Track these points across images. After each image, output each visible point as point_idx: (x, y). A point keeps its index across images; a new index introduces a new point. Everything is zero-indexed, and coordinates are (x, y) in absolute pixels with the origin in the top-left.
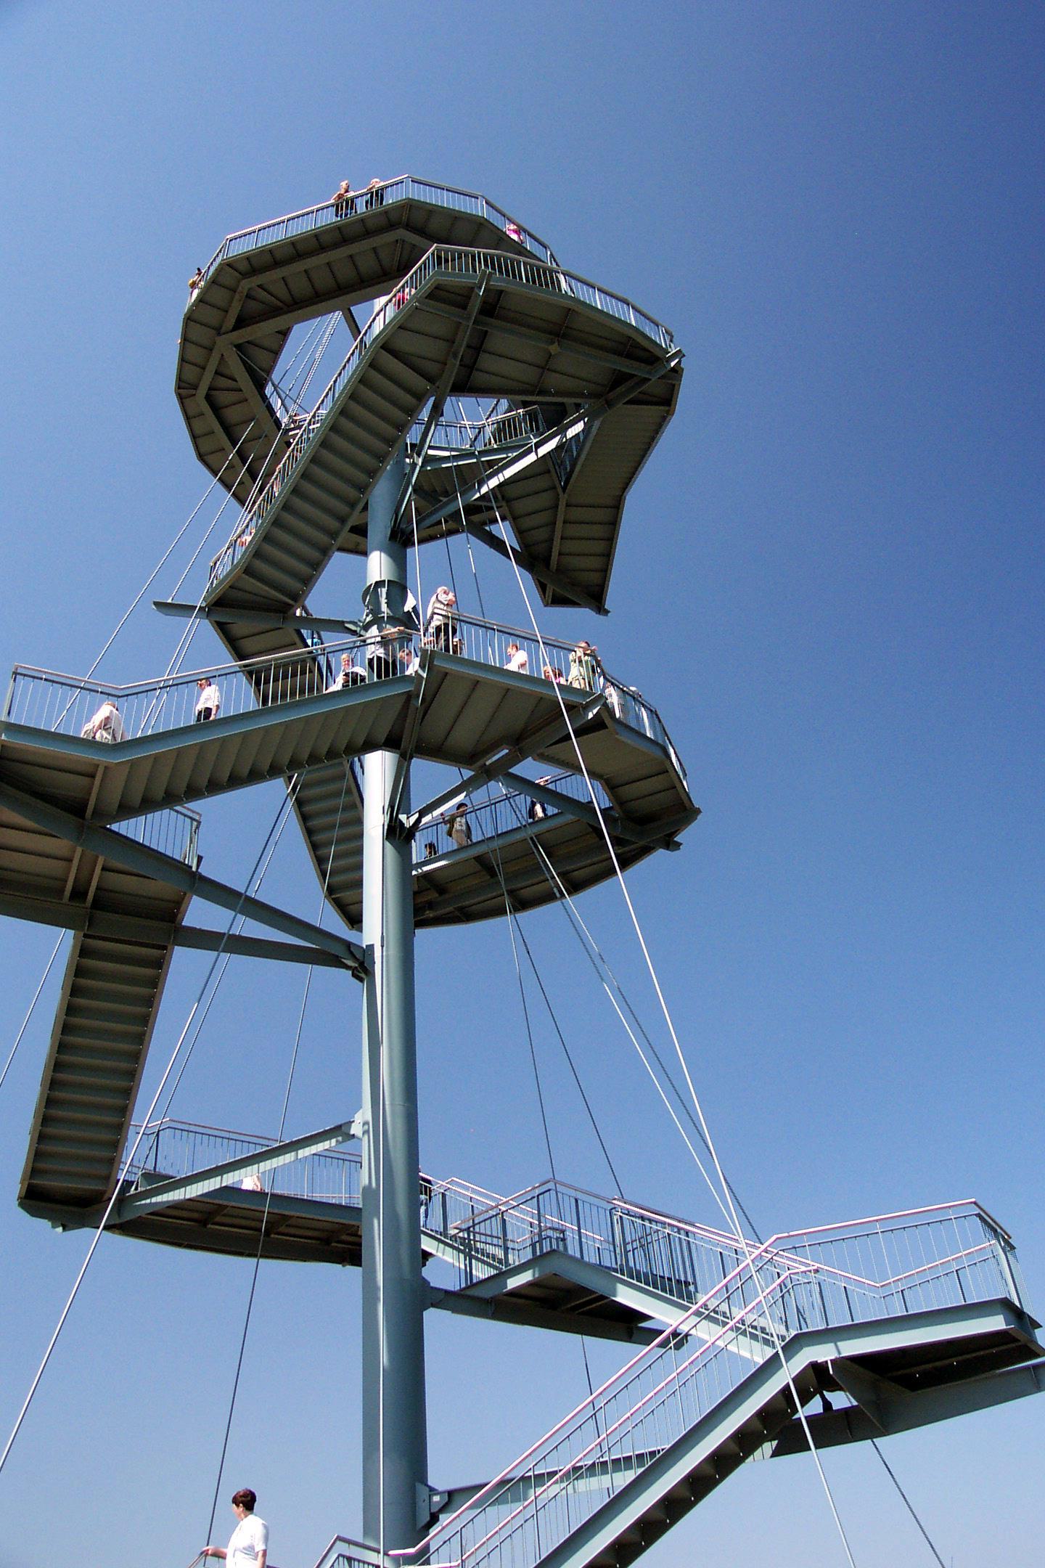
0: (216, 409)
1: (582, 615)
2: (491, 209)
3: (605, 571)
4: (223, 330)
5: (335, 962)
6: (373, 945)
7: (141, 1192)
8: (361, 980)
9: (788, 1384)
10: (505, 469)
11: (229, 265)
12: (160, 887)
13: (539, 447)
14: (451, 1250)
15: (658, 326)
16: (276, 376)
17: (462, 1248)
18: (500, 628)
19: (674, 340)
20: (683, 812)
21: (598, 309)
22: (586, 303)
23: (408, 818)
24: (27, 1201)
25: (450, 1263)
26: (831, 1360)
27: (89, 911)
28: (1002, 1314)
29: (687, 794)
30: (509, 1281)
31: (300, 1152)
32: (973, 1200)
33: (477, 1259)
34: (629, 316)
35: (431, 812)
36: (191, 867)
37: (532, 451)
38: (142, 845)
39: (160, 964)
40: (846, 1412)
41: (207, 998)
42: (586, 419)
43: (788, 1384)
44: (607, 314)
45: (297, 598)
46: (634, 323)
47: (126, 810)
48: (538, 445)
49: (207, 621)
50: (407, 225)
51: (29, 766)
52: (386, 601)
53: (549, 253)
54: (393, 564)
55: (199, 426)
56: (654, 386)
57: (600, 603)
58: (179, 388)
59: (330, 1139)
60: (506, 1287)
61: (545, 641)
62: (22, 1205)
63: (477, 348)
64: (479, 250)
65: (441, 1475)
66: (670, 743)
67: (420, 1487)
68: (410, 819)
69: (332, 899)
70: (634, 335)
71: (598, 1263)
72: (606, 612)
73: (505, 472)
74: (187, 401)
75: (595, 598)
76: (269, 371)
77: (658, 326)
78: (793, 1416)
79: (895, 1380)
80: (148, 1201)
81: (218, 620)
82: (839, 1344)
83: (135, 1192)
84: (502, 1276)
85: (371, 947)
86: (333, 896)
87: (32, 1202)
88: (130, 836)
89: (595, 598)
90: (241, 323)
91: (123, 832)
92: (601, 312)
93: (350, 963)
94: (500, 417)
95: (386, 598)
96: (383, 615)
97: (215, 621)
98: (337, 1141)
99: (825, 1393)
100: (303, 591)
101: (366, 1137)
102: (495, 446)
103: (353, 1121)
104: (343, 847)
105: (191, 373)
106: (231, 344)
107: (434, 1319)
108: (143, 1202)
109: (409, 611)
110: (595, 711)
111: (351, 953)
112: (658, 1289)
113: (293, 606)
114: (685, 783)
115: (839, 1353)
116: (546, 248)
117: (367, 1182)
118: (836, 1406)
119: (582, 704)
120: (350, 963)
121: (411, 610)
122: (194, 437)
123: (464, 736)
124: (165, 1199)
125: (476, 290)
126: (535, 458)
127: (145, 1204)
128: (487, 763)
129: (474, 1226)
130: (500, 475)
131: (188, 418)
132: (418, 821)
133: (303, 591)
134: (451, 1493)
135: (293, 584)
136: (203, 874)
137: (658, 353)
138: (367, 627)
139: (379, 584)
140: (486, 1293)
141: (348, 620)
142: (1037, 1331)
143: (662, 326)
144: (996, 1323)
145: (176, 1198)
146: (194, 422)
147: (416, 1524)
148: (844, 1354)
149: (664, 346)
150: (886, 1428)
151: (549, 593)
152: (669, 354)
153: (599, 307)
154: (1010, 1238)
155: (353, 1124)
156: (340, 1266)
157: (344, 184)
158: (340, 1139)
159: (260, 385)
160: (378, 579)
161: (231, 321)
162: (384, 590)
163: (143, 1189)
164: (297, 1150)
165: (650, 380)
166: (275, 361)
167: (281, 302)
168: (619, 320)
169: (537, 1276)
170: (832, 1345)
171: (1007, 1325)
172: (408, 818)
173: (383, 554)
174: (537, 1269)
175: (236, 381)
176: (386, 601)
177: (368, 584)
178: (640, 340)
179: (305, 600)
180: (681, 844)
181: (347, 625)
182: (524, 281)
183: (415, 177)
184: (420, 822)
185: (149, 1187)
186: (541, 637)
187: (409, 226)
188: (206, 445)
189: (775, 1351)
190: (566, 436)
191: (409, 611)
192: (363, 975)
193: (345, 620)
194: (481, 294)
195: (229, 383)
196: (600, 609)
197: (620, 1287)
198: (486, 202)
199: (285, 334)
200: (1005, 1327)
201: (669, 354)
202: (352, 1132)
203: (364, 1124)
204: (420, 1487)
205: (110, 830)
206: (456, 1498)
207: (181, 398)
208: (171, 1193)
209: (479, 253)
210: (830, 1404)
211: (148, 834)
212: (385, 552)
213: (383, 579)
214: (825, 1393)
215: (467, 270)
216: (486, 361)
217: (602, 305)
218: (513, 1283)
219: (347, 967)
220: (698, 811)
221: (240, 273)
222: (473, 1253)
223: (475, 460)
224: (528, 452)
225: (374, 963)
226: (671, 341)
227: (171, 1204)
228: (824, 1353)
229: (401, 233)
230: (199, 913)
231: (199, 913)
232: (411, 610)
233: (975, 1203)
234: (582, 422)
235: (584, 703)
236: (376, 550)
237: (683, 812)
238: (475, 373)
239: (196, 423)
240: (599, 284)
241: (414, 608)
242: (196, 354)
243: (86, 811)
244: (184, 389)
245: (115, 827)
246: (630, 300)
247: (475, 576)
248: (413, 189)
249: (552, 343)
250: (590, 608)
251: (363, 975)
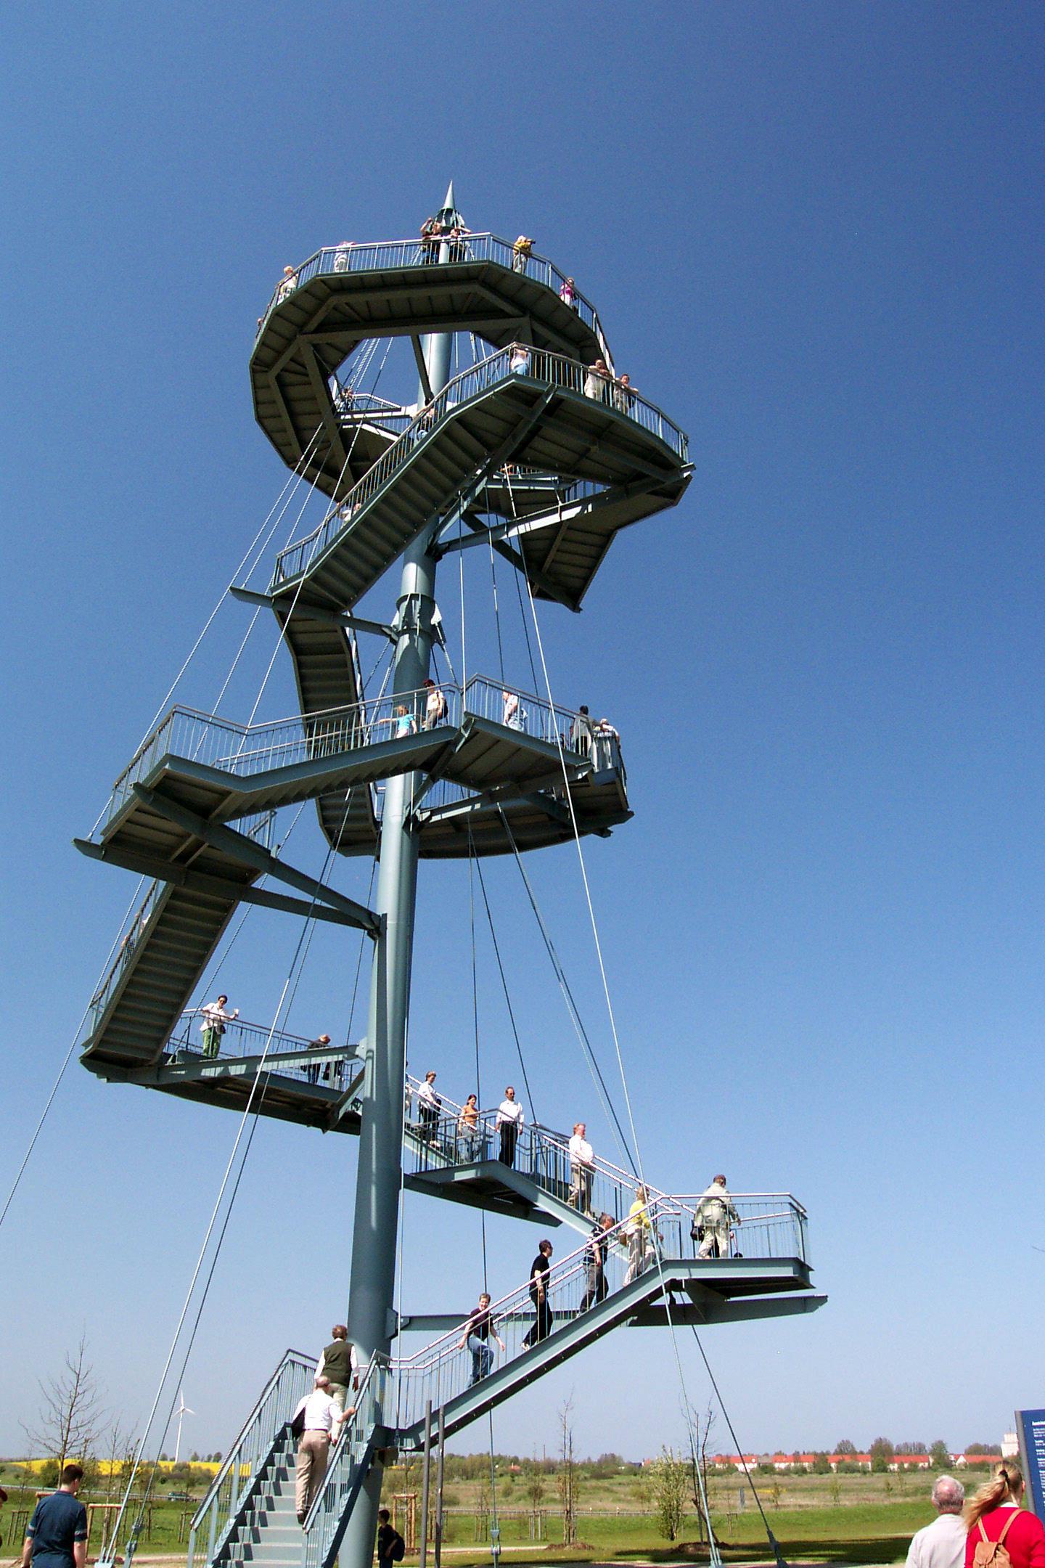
0: (282, 385)
1: (558, 609)
2: (554, 273)
3: (586, 580)
4: (306, 329)
5: (359, 925)
6: (386, 914)
7: (177, 1065)
8: (374, 939)
9: (661, 1287)
10: (532, 521)
11: (322, 281)
13: (565, 510)
15: (678, 432)
19: (689, 444)
20: (621, 812)
24: (88, 1060)
26: (685, 1280)
27: (186, 870)
28: (793, 1266)
30: (456, 1174)
31: (313, 1059)
32: (788, 1193)
34: (658, 424)
35: (441, 814)
36: (269, 852)
38: (239, 834)
39: (228, 910)
40: (684, 1306)
43: (661, 1287)
45: (349, 603)
46: (661, 437)
47: (239, 813)
48: (564, 509)
49: (271, 609)
50: (483, 281)
52: (418, 615)
54: (425, 577)
55: (263, 395)
56: (669, 482)
57: (576, 602)
58: (254, 364)
60: (453, 1179)
61: (557, 709)
65: (404, 1304)
67: (388, 1309)
68: (424, 814)
70: (661, 448)
72: (579, 610)
73: (532, 523)
74: (257, 376)
75: (572, 598)
76: (335, 366)
77: (678, 432)
78: (651, 1302)
79: (717, 1291)
81: (280, 610)
83: (171, 1064)
84: (450, 1170)
89: (572, 598)
90: (320, 329)
91: (232, 827)
92: (638, 425)
94: (493, 355)
95: (419, 613)
96: (415, 627)
99: (673, 1292)
101: (370, 1061)
102: (520, 477)
104: (356, 812)
106: (310, 343)
107: (408, 1198)
108: (179, 1072)
109: (434, 625)
110: (584, 774)
111: (371, 920)
114: (625, 789)
115: (691, 1275)
116: (593, 310)
117: (369, 1095)
118: (679, 1301)
119: (574, 766)
120: (367, 926)
121: (437, 625)
122: (257, 403)
123: (481, 767)
125: (543, 397)
130: (527, 525)
131: (255, 387)
132: (430, 818)
133: (354, 598)
134: (411, 1318)
135: (347, 591)
136: (281, 860)
137: (677, 462)
138: (400, 634)
139: (414, 596)
140: (438, 1180)
141: (385, 624)
142: (810, 1273)
143: (682, 432)
144: (788, 1272)
147: (385, 1332)
151: (537, 586)
152: (685, 466)
153: (637, 421)
154: (805, 1211)
155: (358, 1048)
156: (306, 1126)
157: (605, 720)
158: (346, 1056)
159: (325, 377)
160: (414, 592)
161: (313, 324)
162: (419, 603)
164: (310, 1057)
166: (343, 359)
167: (358, 314)
168: (650, 433)
169: (479, 1175)
170: (687, 1270)
171: (794, 1273)
173: (419, 568)
175: (306, 368)
176: (418, 615)
177: (402, 595)
180: (612, 832)
181: (384, 629)
184: (431, 819)
186: (554, 705)
187: (485, 284)
188: (265, 410)
191: (434, 625)
194: (547, 402)
195: (299, 368)
196: (575, 607)
198: (552, 268)
199: (356, 343)
201: (685, 466)
202: (357, 1053)
203: (368, 1052)
204: (388, 1309)
207: (253, 372)
210: (675, 1300)
212: (422, 568)
213: (417, 593)
216: (538, 443)
217: (639, 420)
218: (459, 1176)
219: (365, 928)
220: (632, 814)
221: (329, 287)
224: (553, 512)
225: (386, 929)
228: (682, 1275)
229: (475, 288)
230: (267, 882)
232: (437, 625)
235: (577, 766)
236: (413, 562)
237: (621, 812)
238: (527, 450)
239: (260, 392)
241: (439, 623)
244: (259, 365)
245: (227, 824)
246: (662, 410)
247: (497, 614)
248: (493, 247)
251: (376, 936)
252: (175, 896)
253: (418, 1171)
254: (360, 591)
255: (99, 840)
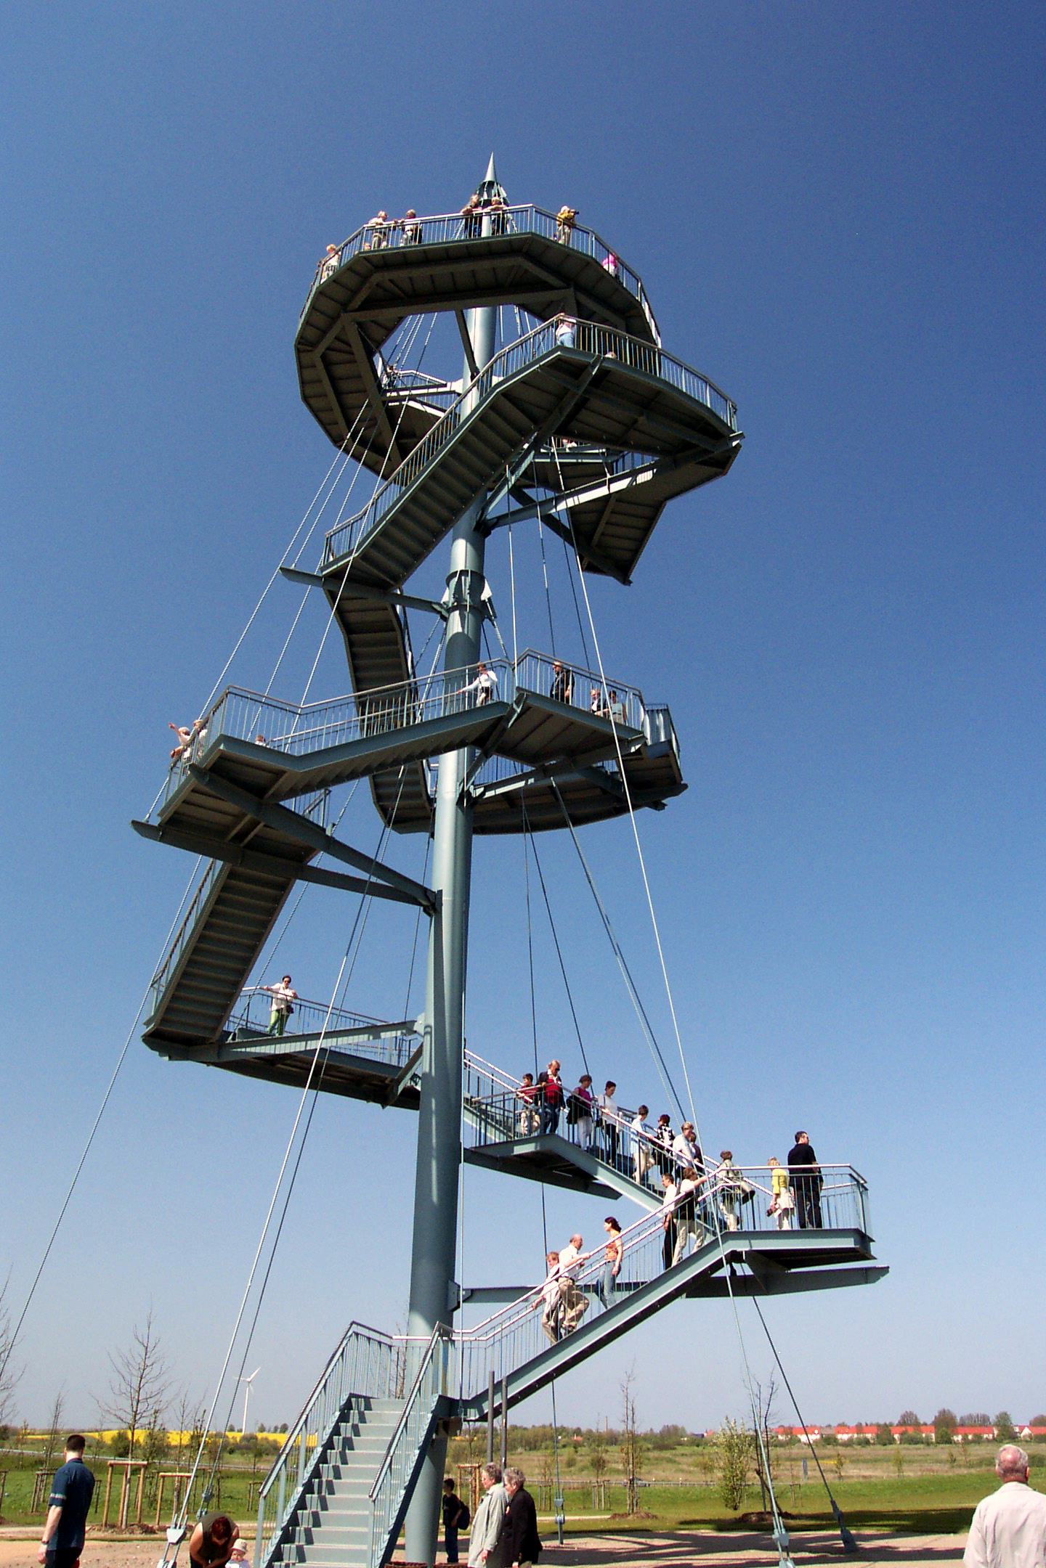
3: (636, 552)
8: (430, 915)
12: (297, 838)
14: (471, 1115)
15: (726, 401)
16: (387, 348)
17: (478, 1114)
18: (575, 670)
20: (674, 785)
21: (682, 391)
22: (674, 386)
23: (475, 789)
25: (469, 1125)
26: (746, 1252)
29: (679, 770)
32: (848, 1165)
33: (492, 1126)
37: (605, 485)
38: (294, 813)
39: (284, 889)
41: (352, 952)
42: (655, 470)
44: (690, 397)
45: (399, 579)
46: (709, 406)
47: (293, 793)
48: (611, 481)
51: (996, 1534)
53: (639, 286)
55: (309, 374)
58: (299, 343)
59: (397, 1030)
60: (513, 1152)
61: (609, 683)
62: (143, 1040)
63: (582, 404)
64: (595, 324)
65: (466, 1277)
66: (673, 729)
69: (380, 805)
71: (571, 1141)
72: (630, 582)
74: (302, 355)
75: (622, 571)
76: (380, 343)
77: (726, 401)
80: (243, 1050)
82: (752, 1241)
83: (231, 1042)
84: (510, 1144)
85: (440, 892)
86: (381, 803)
87: (152, 1040)
88: (287, 807)
89: (622, 571)
93: (424, 903)
97: (329, 591)
98: (402, 1033)
99: (733, 1264)
100: (404, 576)
101: (428, 1037)
103: (416, 1021)
105: (312, 333)
107: (469, 1174)
108: (239, 1050)
109: (485, 601)
110: (637, 747)
112: (621, 1171)
113: (392, 586)
117: (427, 1070)
118: (739, 1273)
122: (303, 383)
123: (534, 742)
124: (263, 1051)
125: (590, 368)
126: (607, 493)
127: (241, 1052)
128: (546, 764)
129: (492, 1103)
130: (576, 498)
132: (483, 793)
134: (473, 1291)
135: (395, 568)
137: (722, 429)
139: (463, 573)
140: (497, 1153)
142: (871, 1243)
145: (268, 1052)
146: (304, 371)
148: (754, 1249)
149: (729, 425)
150: (768, 1291)
153: (684, 390)
154: (866, 1182)
155: (416, 1024)
158: (404, 1031)
160: (463, 568)
161: (357, 302)
162: (469, 579)
163: (240, 1040)
165: (713, 452)
170: (747, 1241)
171: (855, 1245)
172: (475, 789)
174: (539, 1144)
175: (350, 346)
177: (452, 571)
178: (713, 421)
179: (403, 584)
182: (628, 363)
183: (541, 208)
184: (484, 795)
185: (246, 1040)
189: (714, 1238)
190: (636, 480)
191: (485, 601)
192: (431, 912)
193: (433, 601)
196: (625, 580)
197: (600, 1170)
198: (595, 238)
199: (401, 319)
200: (853, 1246)
202: (415, 1029)
205: (281, 806)
206: (477, 1295)
207: (298, 351)
208: (263, 1047)
209: (594, 327)
210: (735, 1271)
211: (297, 806)
214: (733, 1264)
215: (584, 348)
218: (519, 1150)
219: (420, 904)
220: (685, 786)
222: (489, 1120)
223: (549, 460)
226: (735, 413)
227: (258, 1056)
228: (742, 1246)
230: (322, 861)
231: (322, 861)
233: (850, 1167)
234: (651, 472)
236: (463, 538)
237: (674, 785)
240: (689, 364)
241: (489, 599)
242: (320, 320)
243: (265, 794)
244: (304, 345)
245: (282, 803)
249: (641, 414)
250: (614, 577)
251: (431, 912)
252: (232, 875)
253: (478, 1145)
254: (409, 568)
255: (156, 822)
